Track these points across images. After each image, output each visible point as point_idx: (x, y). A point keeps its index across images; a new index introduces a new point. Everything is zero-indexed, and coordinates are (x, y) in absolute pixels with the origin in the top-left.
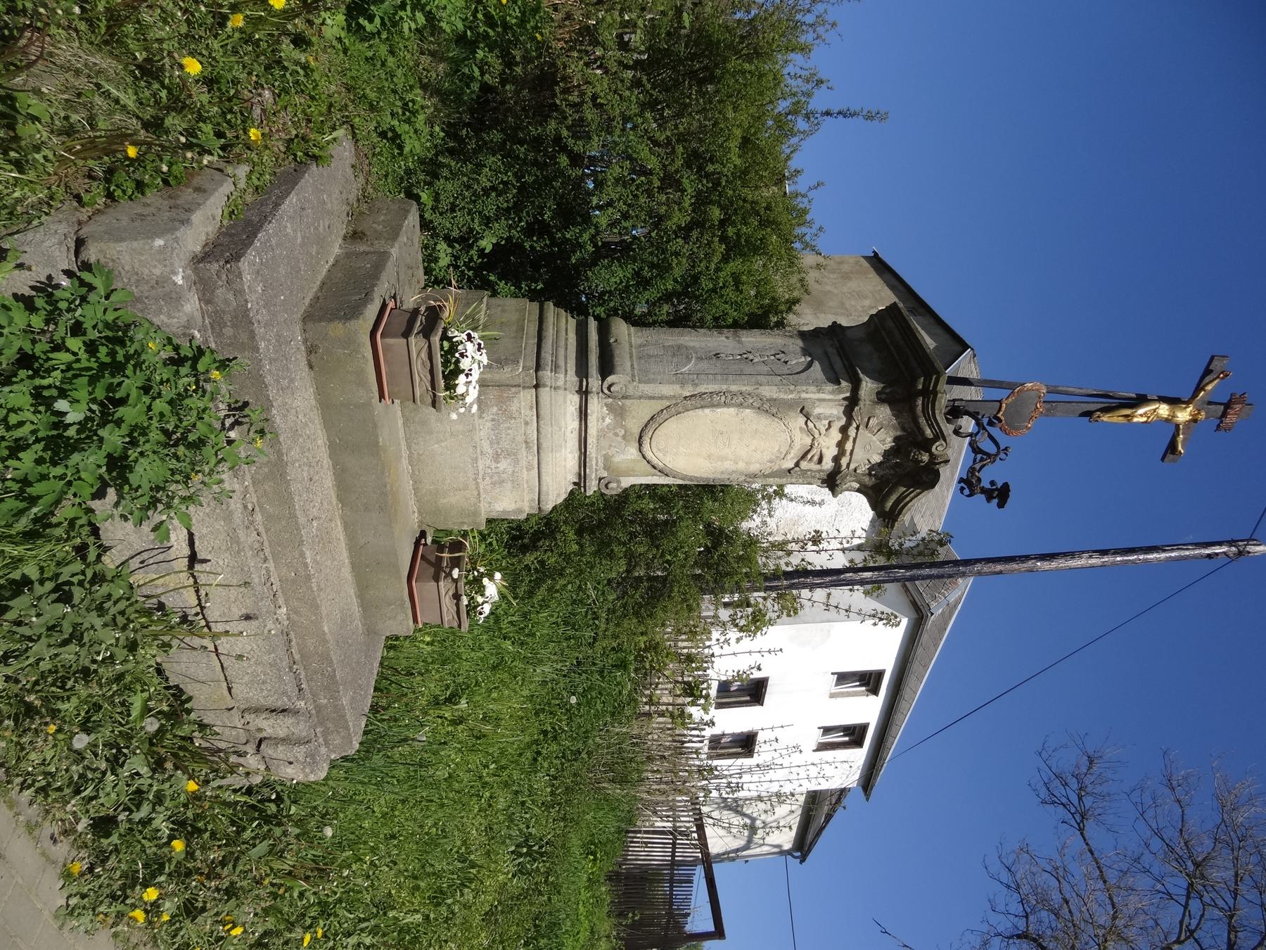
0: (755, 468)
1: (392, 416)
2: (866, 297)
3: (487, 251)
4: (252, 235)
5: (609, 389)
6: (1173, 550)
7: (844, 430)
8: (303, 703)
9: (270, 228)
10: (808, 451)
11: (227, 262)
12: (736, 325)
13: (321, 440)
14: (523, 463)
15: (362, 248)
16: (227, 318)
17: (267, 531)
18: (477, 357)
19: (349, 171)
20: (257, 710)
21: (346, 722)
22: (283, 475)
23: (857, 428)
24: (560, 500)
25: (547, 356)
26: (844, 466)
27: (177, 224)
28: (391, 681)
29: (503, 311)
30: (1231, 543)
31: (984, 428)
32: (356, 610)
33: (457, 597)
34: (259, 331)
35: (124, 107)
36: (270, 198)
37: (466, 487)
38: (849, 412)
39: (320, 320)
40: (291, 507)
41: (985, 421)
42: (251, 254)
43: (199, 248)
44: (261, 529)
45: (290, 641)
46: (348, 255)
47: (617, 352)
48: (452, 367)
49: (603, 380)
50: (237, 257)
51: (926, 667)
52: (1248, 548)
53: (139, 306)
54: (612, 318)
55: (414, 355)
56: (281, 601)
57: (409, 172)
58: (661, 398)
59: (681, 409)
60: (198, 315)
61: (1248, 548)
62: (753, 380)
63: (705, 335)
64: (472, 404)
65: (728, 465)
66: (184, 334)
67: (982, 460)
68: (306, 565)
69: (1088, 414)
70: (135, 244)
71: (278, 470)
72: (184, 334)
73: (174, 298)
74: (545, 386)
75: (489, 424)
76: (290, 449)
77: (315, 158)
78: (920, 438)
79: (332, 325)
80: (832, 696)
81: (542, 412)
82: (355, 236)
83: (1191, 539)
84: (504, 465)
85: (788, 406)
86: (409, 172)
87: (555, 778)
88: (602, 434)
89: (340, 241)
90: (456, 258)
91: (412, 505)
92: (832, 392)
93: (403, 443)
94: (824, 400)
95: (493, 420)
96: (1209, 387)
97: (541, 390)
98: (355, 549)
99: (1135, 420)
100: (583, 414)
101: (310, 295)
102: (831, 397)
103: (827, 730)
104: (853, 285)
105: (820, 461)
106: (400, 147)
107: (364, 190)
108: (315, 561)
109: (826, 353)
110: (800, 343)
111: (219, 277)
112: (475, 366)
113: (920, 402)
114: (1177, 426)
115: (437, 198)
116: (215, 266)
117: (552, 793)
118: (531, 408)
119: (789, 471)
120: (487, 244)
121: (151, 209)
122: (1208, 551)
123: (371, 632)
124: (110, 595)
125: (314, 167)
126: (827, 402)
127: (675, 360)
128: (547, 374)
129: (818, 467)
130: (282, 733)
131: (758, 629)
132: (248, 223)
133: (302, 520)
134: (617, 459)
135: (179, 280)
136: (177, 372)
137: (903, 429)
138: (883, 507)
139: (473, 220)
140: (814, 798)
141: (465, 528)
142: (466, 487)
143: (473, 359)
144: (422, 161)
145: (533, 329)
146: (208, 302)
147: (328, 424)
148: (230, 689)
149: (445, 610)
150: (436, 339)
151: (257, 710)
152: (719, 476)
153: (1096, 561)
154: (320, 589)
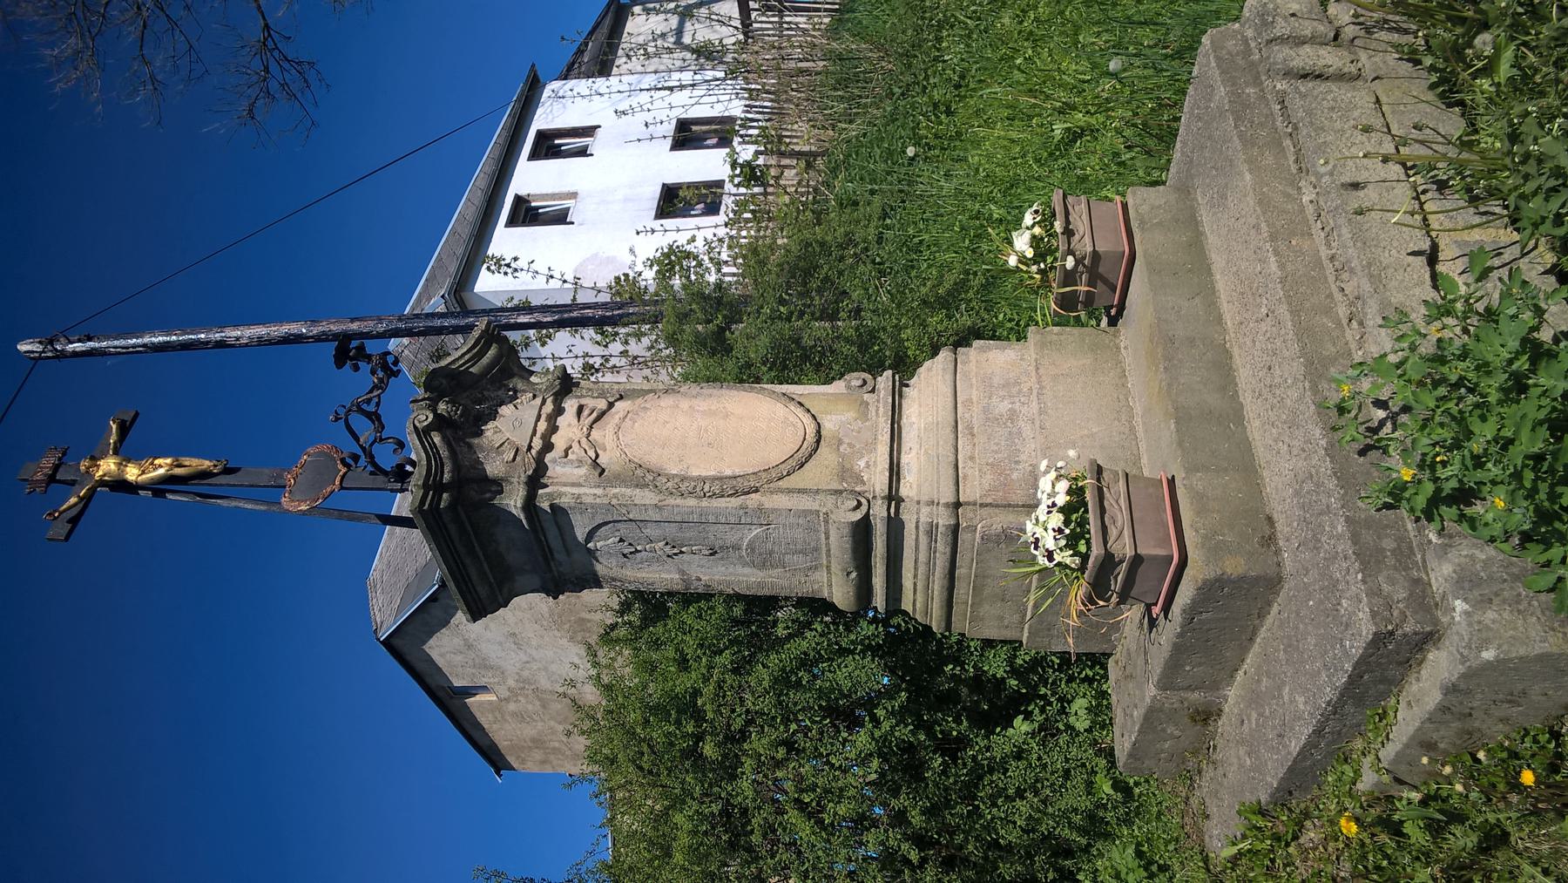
0: (667, 401)
1: (1156, 457)
2: (514, 714)
3: (1021, 717)
4: (1354, 679)
5: (859, 504)
6: (134, 346)
7: (548, 447)
8: (1279, 86)
9: (1329, 694)
10: (595, 421)
11: (1391, 633)
12: (688, 599)
13: (1255, 430)
14: (976, 409)
15: (1195, 696)
16: (1391, 561)
17: (1330, 296)
18: (1039, 531)
19: (1213, 810)
20: (1340, 77)
21: (1219, 66)
22: (1309, 363)
23: (530, 448)
24: (927, 364)
25: (942, 547)
26: (549, 401)
27: (1463, 686)
28: (1157, 137)
29: (1001, 618)
30: (63, 355)
31: (364, 449)
32: (1205, 216)
33: (1069, 232)
34: (1346, 547)
35: (1535, 864)
36: (1327, 745)
37: (1055, 378)
38: (541, 468)
39: (1257, 579)
40: (1297, 324)
41: (363, 461)
42: (1356, 647)
43: (1430, 656)
44: (1338, 296)
45: (1297, 161)
46: (1215, 686)
47: (848, 556)
48: (1074, 517)
49: (867, 515)
50: (1379, 640)
51: (453, 232)
52: (40, 348)
53: (1515, 570)
54: (854, 609)
55: (1127, 533)
56: (1310, 209)
57: (1128, 822)
58: (790, 491)
59: (764, 475)
60: (1432, 563)
61: (40, 348)
62: (665, 515)
63: (729, 584)
64: (1047, 472)
65: (702, 405)
66: (1451, 537)
67: (369, 401)
68: (1276, 253)
69: (228, 471)
70: (1522, 652)
71: (1315, 370)
72: (1451, 537)
73: (1465, 582)
74: (947, 505)
75: (1023, 457)
76: (1301, 399)
77: (1262, 813)
78: (448, 433)
79: (1240, 571)
80: (573, 195)
81: (951, 471)
82: (1206, 716)
83: (109, 361)
84: (1003, 407)
85: (619, 479)
86: (1128, 822)
87: (936, 59)
88: (871, 446)
89: (1226, 709)
90: (1063, 711)
91: (1127, 357)
92: (560, 495)
93: (1140, 434)
94: (573, 485)
95: (1017, 462)
96: (73, 500)
97: (952, 499)
98: (1209, 294)
99: (169, 461)
100: (895, 471)
101: (1269, 620)
102: (564, 489)
103: (583, 152)
104: (529, 731)
105: (580, 409)
106: (1139, 854)
107: (1191, 787)
108: (1263, 261)
109: (568, 552)
110: (600, 569)
111: (1403, 613)
112: (1042, 518)
113: (447, 477)
114: (116, 453)
115: (1090, 785)
116: (1408, 628)
117: (939, 40)
118: (965, 477)
119: (621, 397)
120: (1021, 726)
121: (1498, 712)
122: (91, 344)
123: (1185, 190)
124: (1547, 200)
125: (1264, 798)
126: (567, 481)
127: (769, 546)
128: (944, 519)
129: (583, 401)
130: (1307, 49)
131: (667, 255)
132: (1360, 701)
133: (1283, 311)
134: (851, 415)
135: (1459, 605)
136: (1460, 481)
137: (470, 446)
138: (500, 349)
139: (1039, 758)
140: (603, 68)
141: (1056, 329)
142: (1055, 378)
143: (1044, 529)
144: (1107, 836)
145: (962, 591)
146: (1417, 581)
147: (1246, 447)
148: (1378, 101)
149: (1085, 217)
150: (1096, 551)
151: (1340, 77)
152: (715, 392)
153: (232, 333)
154: (1257, 227)
